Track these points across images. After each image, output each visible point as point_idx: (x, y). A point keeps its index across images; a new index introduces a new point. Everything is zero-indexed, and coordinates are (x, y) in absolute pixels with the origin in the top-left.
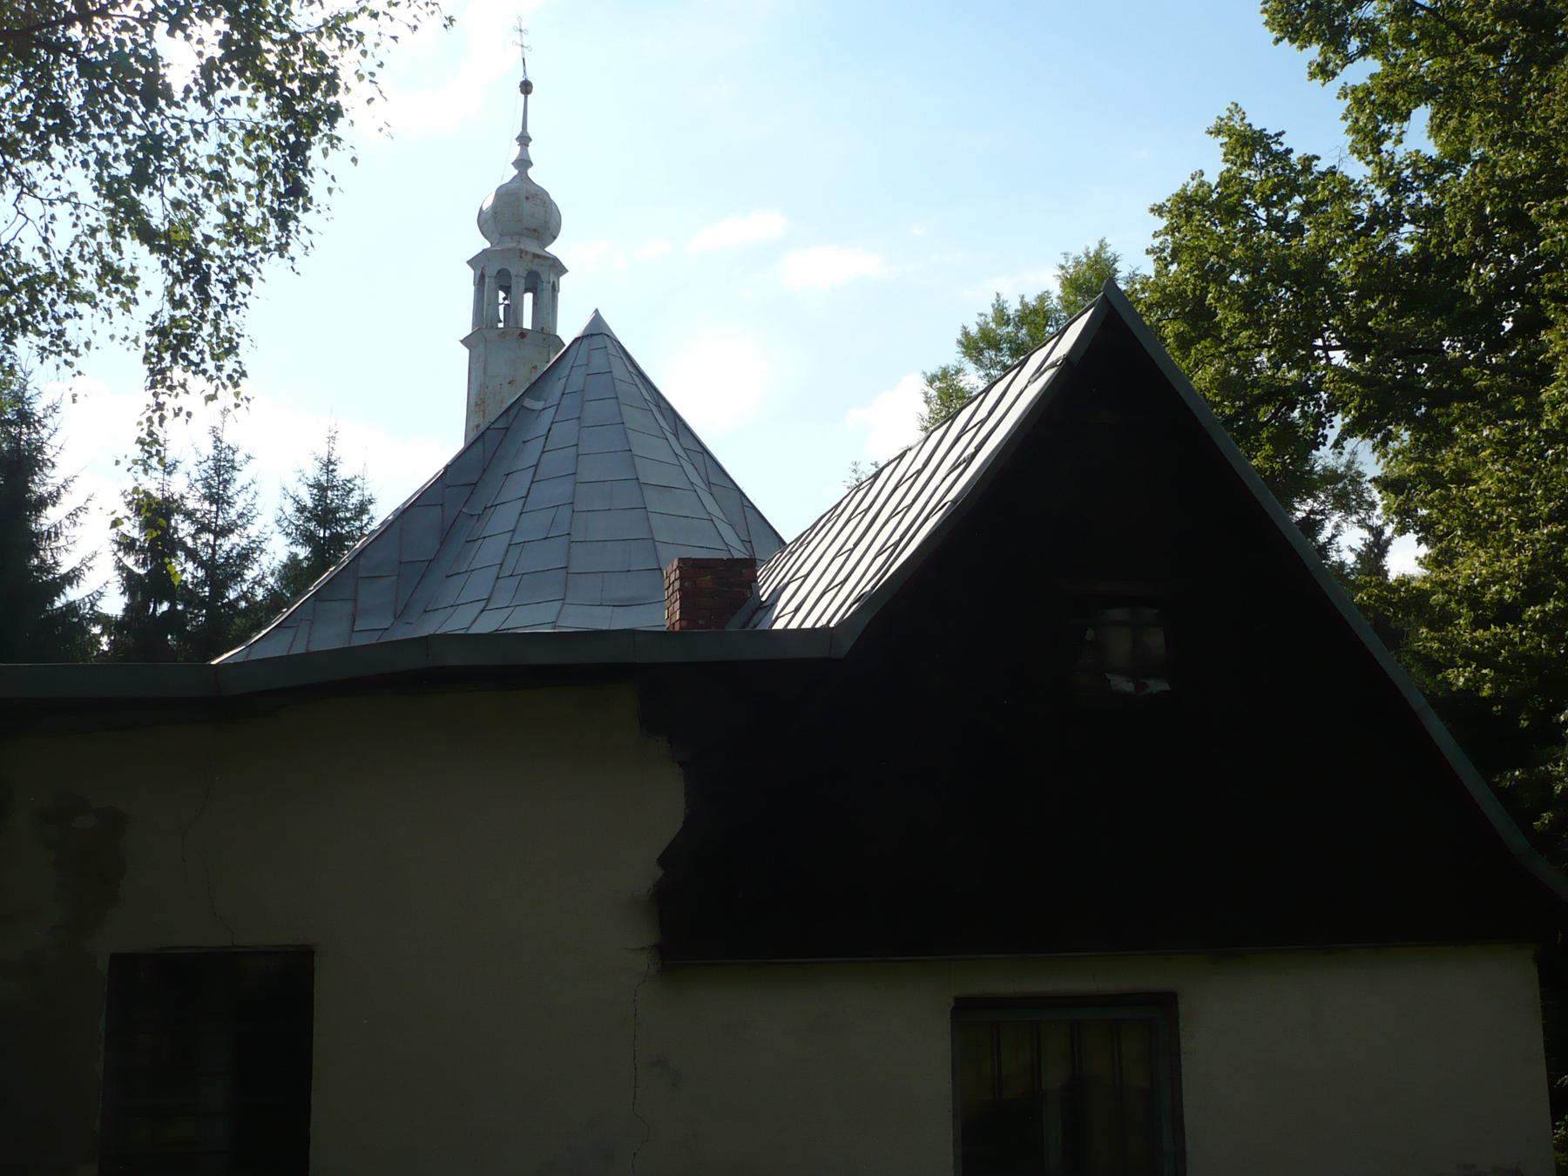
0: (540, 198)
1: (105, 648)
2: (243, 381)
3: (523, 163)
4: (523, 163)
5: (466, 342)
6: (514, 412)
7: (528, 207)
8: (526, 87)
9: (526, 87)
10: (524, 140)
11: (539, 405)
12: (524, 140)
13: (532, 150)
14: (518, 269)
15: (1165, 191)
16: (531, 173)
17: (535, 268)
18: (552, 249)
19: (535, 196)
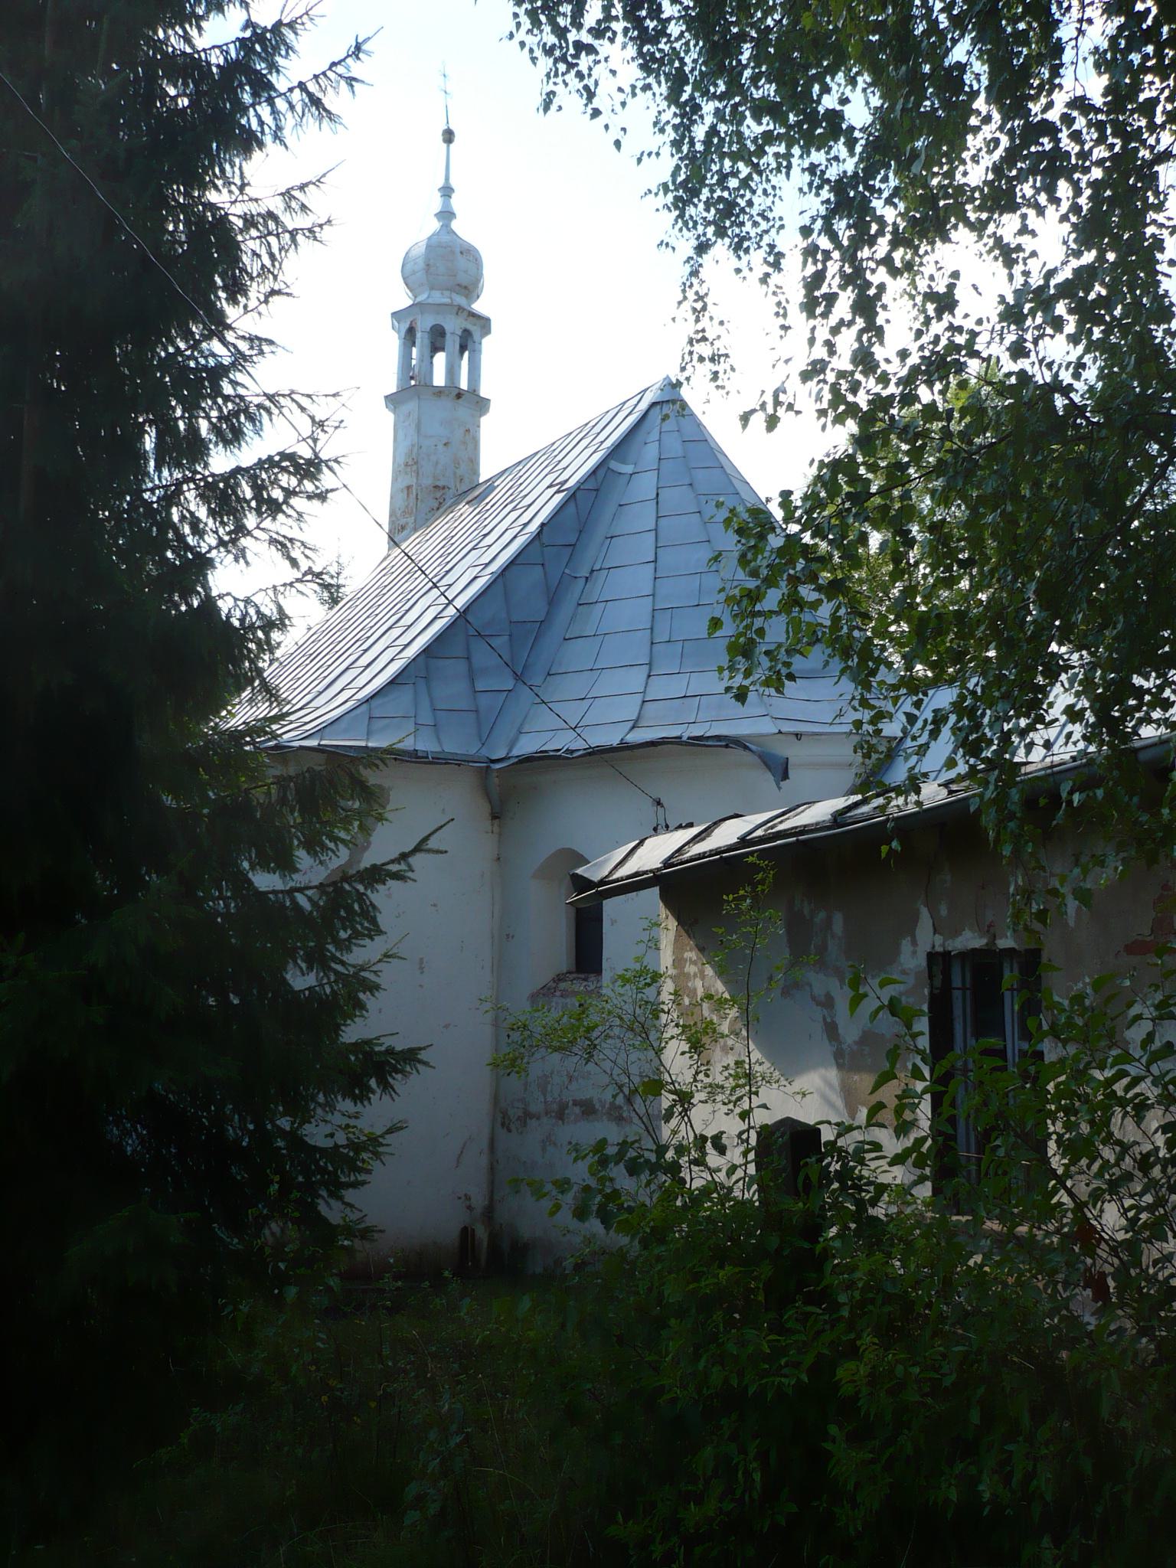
0: (471, 255)
1: (1054, 647)
2: (707, 335)
3: (446, 215)
4: (446, 215)
5: (392, 401)
6: (601, 473)
7: (462, 262)
8: (449, 136)
9: (449, 136)
10: (447, 191)
11: (628, 469)
12: (447, 191)
13: (456, 202)
14: (453, 326)
15: (493, 406)
16: (455, 225)
17: (469, 327)
18: (478, 307)
19: (468, 251)
